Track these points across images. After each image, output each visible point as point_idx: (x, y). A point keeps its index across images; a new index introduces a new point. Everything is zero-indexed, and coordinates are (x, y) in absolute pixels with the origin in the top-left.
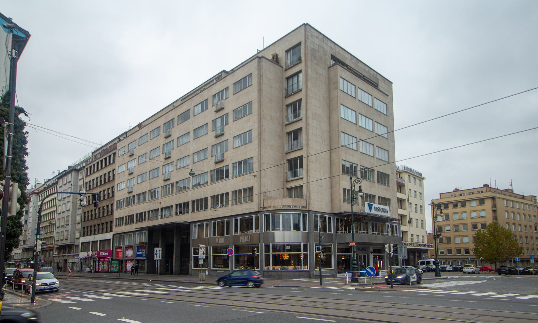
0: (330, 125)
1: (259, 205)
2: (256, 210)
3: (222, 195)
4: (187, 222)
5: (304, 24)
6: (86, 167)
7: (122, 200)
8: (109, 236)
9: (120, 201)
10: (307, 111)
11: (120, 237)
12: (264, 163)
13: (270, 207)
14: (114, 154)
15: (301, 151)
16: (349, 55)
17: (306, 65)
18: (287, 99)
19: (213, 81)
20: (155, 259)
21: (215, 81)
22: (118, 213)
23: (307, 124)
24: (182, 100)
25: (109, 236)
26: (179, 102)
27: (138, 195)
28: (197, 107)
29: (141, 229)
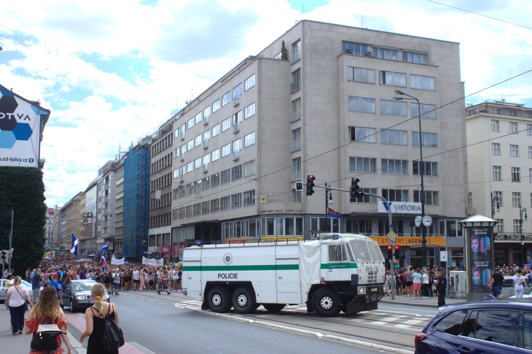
0: (339, 119)
1: (259, 208)
2: (256, 214)
3: (238, 195)
4: (217, 220)
5: (302, 21)
6: (152, 146)
7: (217, 175)
8: (167, 230)
9: (214, 175)
10: (304, 111)
11: (239, 223)
12: (263, 166)
13: (273, 211)
14: (172, 134)
15: (298, 152)
16: (375, 32)
17: (304, 63)
18: (293, 95)
19: (234, 71)
20: (442, 260)
21: (237, 72)
22: (176, 204)
23: (305, 125)
24: (222, 82)
25: (167, 230)
26: (219, 84)
27: (244, 164)
28: (234, 90)
29: (185, 226)
